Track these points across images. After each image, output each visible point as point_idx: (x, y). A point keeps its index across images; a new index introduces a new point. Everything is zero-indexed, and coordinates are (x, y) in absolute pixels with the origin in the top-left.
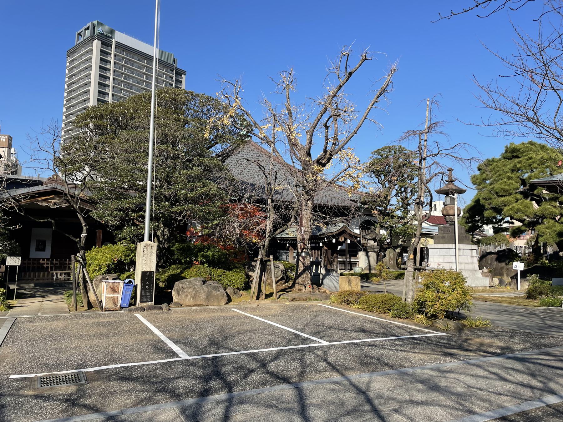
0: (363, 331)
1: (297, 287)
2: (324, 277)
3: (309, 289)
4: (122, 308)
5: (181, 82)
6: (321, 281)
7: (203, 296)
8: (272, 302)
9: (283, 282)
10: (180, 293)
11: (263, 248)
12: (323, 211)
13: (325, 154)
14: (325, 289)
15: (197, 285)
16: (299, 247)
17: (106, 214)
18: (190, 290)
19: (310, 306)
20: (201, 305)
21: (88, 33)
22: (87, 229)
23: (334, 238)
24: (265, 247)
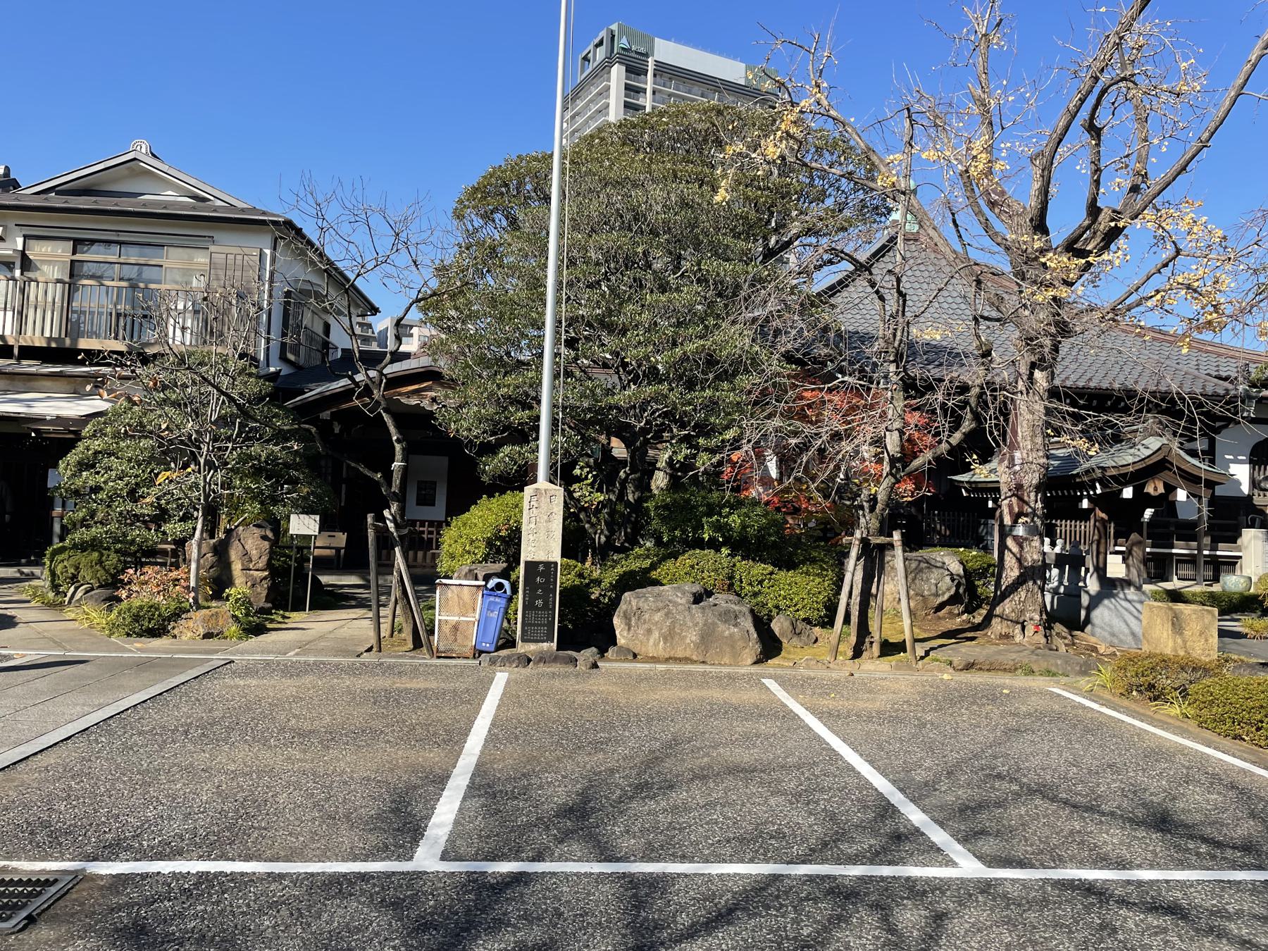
0: (1162, 821)
1: (997, 626)
2: (1096, 601)
3: (1032, 636)
4: (481, 652)
6: (1083, 613)
7: (692, 636)
8: (898, 668)
9: (958, 609)
10: (633, 623)
11: (872, 509)
12: (1099, 407)
13: (1094, 221)
14: (1093, 640)
15: (676, 604)
16: (1006, 511)
17: (463, 415)
18: (658, 617)
19: (1016, 694)
20: (687, 660)
21: (601, 54)
22: (403, 449)
23: (1126, 485)
24: (879, 506)
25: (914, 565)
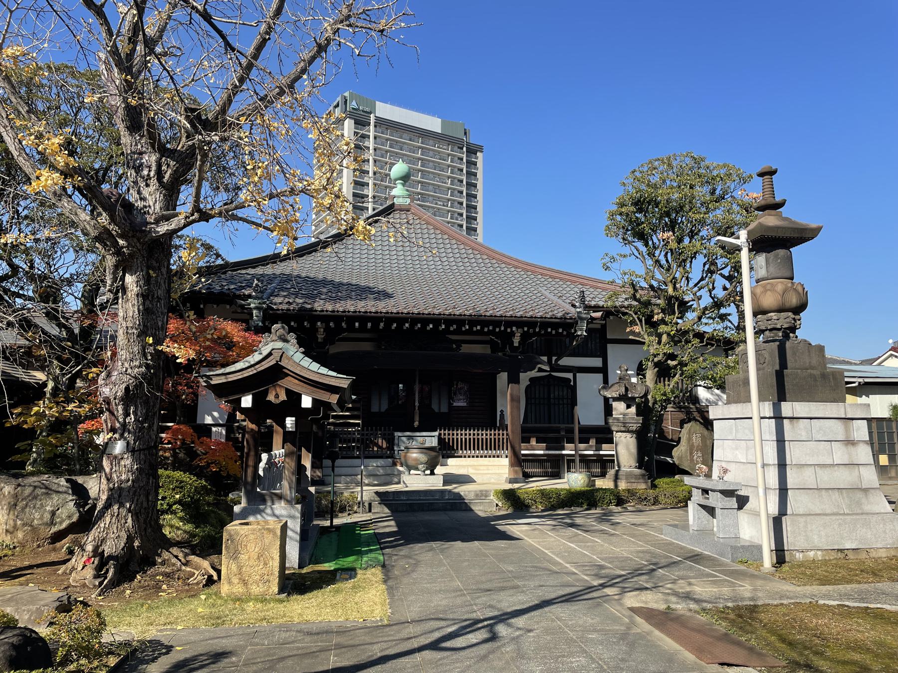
5: (475, 164)
23: (245, 392)
25: (28, 491)
